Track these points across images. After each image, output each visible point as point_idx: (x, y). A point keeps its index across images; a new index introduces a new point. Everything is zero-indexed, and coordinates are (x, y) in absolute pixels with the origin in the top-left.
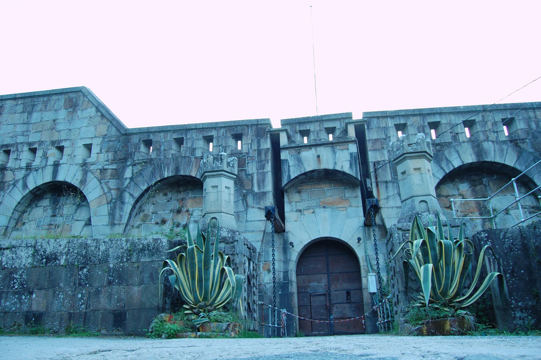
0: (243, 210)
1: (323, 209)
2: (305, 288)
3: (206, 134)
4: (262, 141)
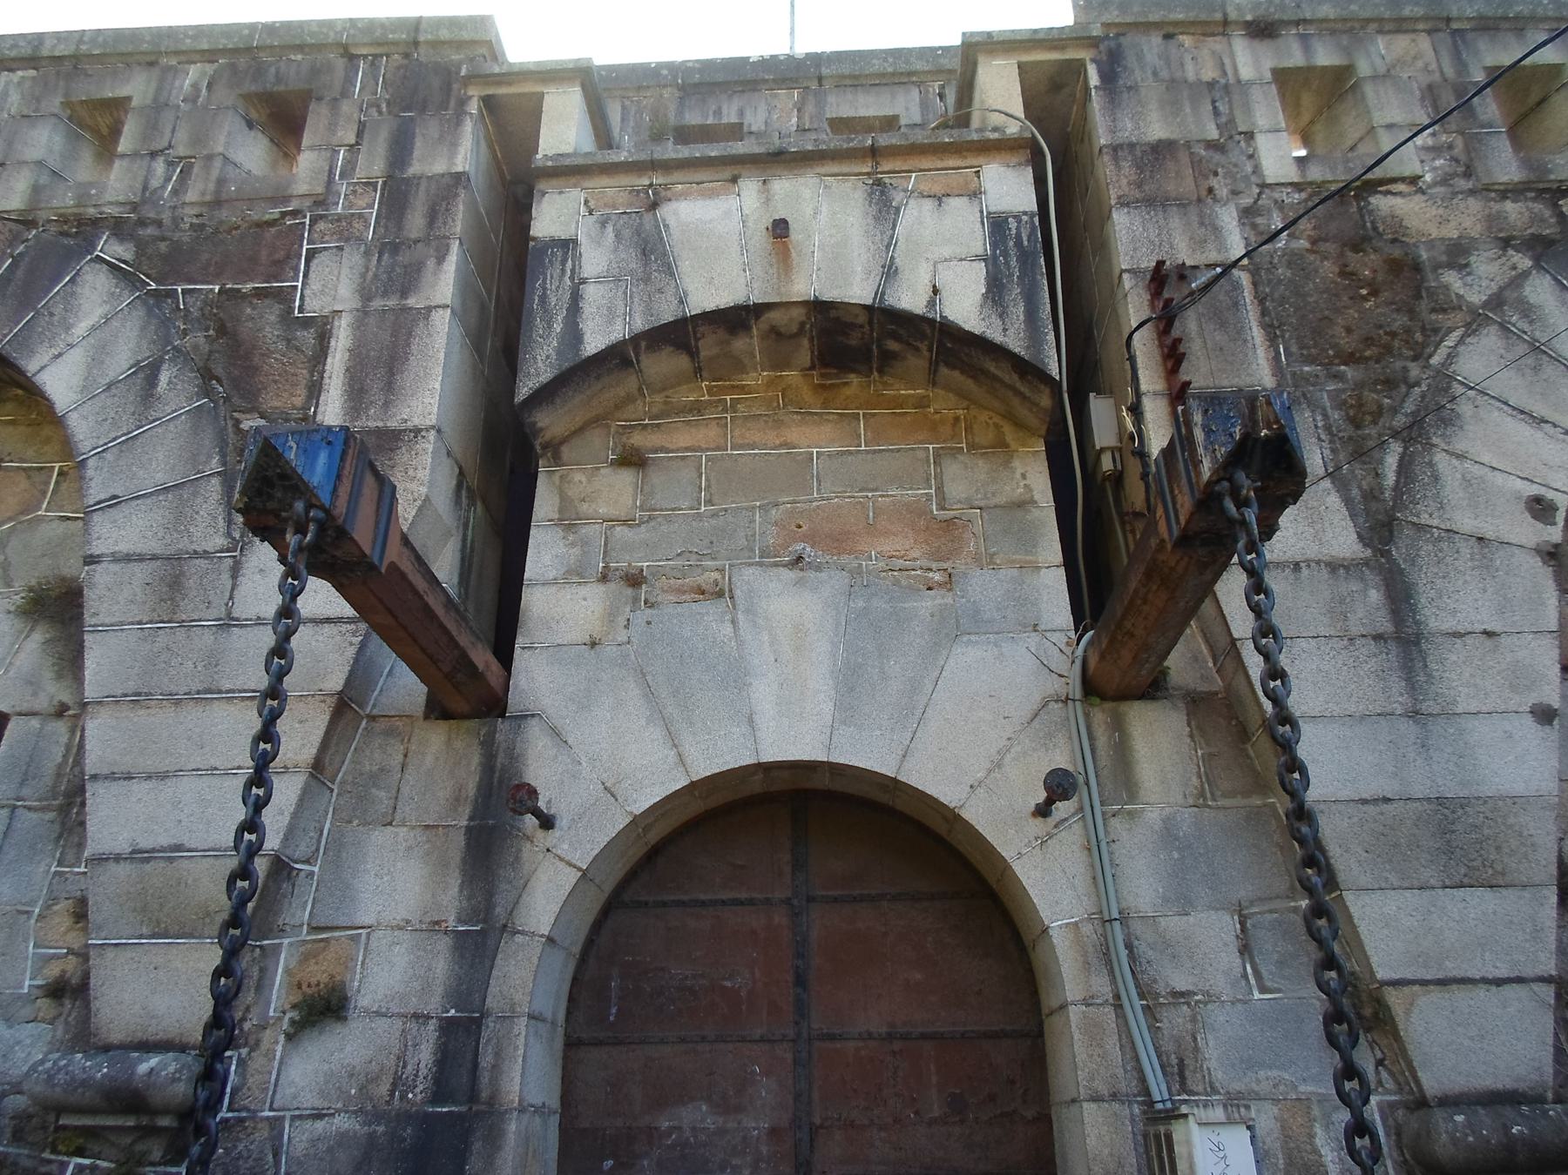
0: (220, 541)
1: (788, 575)
3: (86, 90)
4: (426, 132)
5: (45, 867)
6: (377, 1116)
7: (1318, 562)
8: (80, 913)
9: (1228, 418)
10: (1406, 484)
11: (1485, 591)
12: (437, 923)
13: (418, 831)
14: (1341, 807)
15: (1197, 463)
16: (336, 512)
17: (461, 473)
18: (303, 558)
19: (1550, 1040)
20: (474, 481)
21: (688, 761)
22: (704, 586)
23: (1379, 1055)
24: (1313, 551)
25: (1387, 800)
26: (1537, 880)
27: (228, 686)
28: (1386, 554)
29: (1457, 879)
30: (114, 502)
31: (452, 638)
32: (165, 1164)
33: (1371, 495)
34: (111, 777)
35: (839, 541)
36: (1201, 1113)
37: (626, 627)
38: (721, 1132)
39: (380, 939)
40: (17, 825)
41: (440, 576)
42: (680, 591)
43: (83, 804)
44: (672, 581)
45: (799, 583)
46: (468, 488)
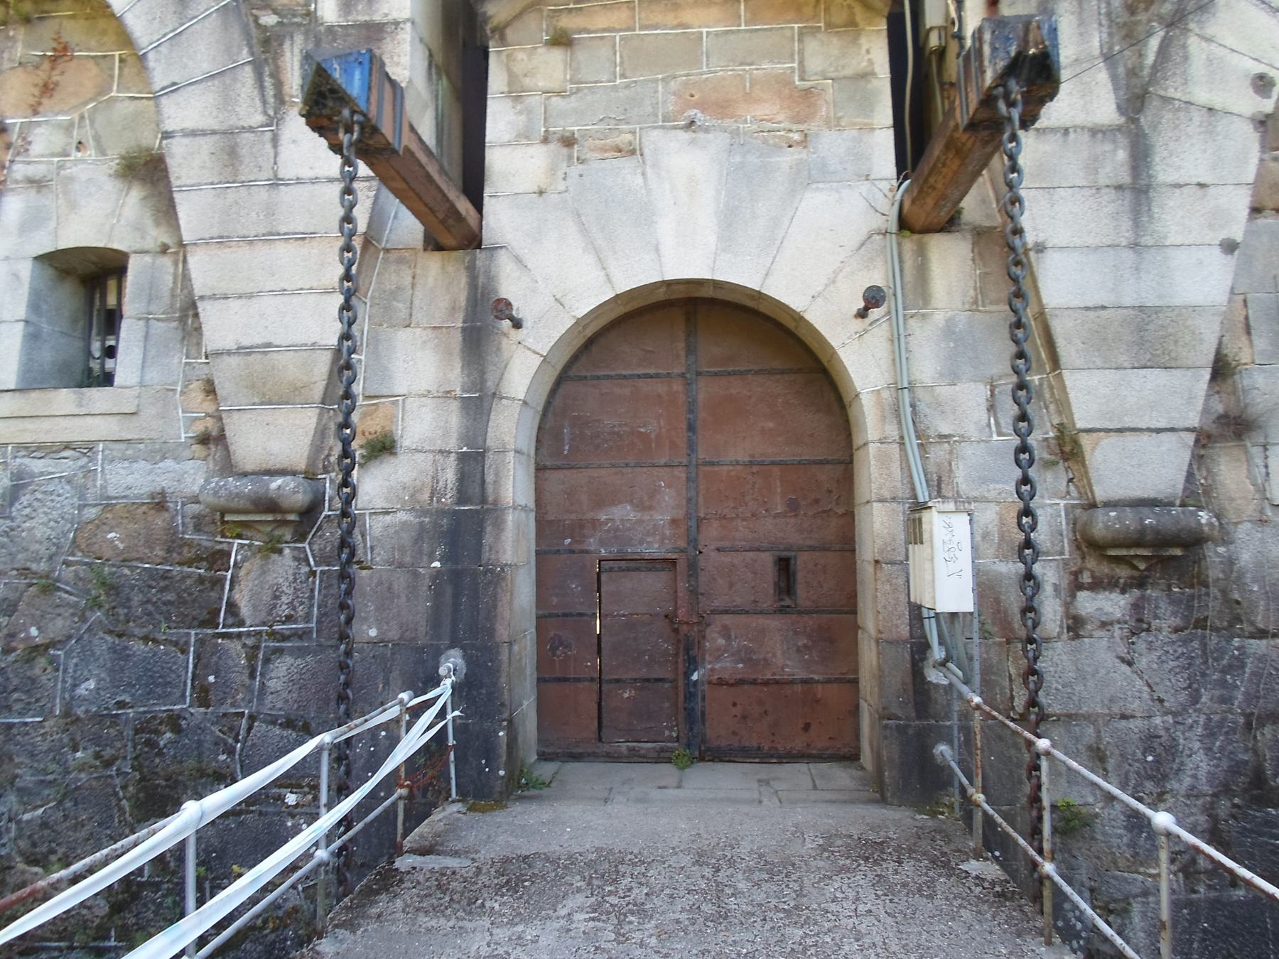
0: (258, 118)
1: (684, 136)
2: (579, 529)
5: (177, 360)
6: (424, 512)
7: (1083, 128)
8: (210, 389)
9: (1008, 39)
10: (1162, 63)
11: (1205, 152)
12: (448, 392)
13: (429, 331)
14: (1070, 312)
15: (983, 72)
16: (371, 116)
17: (431, 55)
18: (353, 149)
19: (1185, 468)
20: (439, 59)
21: (614, 280)
22: (622, 146)
23: (1071, 476)
24: (1081, 119)
25: (1103, 308)
26: (1198, 364)
27: (284, 230)
28: (1134, 121)
29: (1143, 363)
30: (174, 88)
31: (444, 195)
32: (294, 542)
33: (1133, 73)
34: (213, 297)
35: (721, 107)
36: (941, 507)
37: (564, 179)
38: (640, 522)
39: (412, 403)
40: (152, 331)
41: (428, 143)
42: (604, 149)
43: (196, 315)
44: (597, 142)
45: (692, 142)
46: (437, 66)
